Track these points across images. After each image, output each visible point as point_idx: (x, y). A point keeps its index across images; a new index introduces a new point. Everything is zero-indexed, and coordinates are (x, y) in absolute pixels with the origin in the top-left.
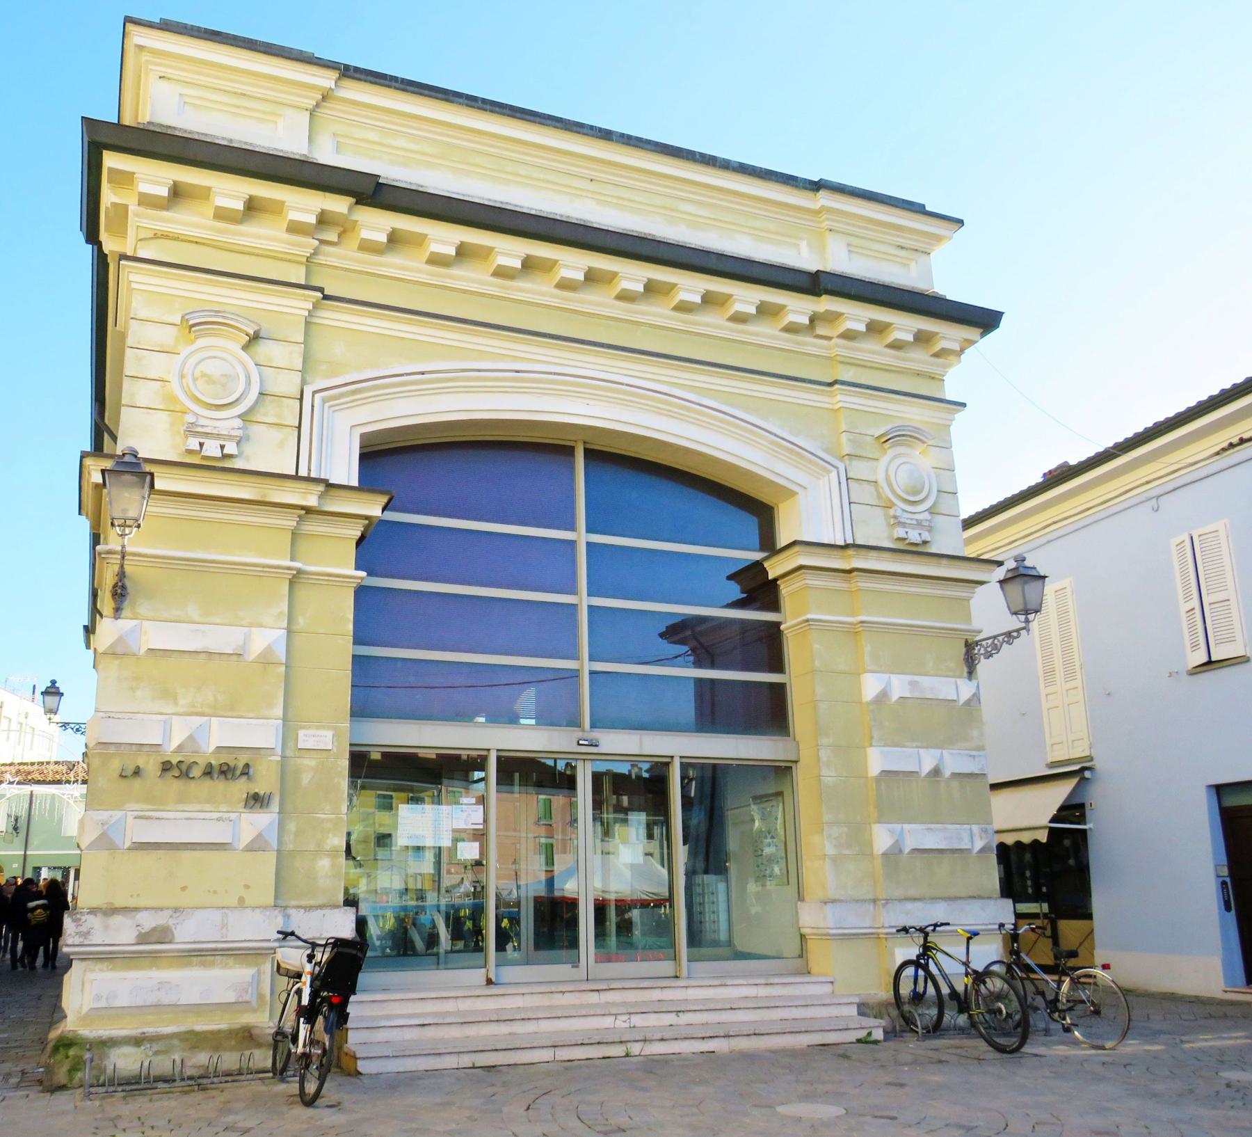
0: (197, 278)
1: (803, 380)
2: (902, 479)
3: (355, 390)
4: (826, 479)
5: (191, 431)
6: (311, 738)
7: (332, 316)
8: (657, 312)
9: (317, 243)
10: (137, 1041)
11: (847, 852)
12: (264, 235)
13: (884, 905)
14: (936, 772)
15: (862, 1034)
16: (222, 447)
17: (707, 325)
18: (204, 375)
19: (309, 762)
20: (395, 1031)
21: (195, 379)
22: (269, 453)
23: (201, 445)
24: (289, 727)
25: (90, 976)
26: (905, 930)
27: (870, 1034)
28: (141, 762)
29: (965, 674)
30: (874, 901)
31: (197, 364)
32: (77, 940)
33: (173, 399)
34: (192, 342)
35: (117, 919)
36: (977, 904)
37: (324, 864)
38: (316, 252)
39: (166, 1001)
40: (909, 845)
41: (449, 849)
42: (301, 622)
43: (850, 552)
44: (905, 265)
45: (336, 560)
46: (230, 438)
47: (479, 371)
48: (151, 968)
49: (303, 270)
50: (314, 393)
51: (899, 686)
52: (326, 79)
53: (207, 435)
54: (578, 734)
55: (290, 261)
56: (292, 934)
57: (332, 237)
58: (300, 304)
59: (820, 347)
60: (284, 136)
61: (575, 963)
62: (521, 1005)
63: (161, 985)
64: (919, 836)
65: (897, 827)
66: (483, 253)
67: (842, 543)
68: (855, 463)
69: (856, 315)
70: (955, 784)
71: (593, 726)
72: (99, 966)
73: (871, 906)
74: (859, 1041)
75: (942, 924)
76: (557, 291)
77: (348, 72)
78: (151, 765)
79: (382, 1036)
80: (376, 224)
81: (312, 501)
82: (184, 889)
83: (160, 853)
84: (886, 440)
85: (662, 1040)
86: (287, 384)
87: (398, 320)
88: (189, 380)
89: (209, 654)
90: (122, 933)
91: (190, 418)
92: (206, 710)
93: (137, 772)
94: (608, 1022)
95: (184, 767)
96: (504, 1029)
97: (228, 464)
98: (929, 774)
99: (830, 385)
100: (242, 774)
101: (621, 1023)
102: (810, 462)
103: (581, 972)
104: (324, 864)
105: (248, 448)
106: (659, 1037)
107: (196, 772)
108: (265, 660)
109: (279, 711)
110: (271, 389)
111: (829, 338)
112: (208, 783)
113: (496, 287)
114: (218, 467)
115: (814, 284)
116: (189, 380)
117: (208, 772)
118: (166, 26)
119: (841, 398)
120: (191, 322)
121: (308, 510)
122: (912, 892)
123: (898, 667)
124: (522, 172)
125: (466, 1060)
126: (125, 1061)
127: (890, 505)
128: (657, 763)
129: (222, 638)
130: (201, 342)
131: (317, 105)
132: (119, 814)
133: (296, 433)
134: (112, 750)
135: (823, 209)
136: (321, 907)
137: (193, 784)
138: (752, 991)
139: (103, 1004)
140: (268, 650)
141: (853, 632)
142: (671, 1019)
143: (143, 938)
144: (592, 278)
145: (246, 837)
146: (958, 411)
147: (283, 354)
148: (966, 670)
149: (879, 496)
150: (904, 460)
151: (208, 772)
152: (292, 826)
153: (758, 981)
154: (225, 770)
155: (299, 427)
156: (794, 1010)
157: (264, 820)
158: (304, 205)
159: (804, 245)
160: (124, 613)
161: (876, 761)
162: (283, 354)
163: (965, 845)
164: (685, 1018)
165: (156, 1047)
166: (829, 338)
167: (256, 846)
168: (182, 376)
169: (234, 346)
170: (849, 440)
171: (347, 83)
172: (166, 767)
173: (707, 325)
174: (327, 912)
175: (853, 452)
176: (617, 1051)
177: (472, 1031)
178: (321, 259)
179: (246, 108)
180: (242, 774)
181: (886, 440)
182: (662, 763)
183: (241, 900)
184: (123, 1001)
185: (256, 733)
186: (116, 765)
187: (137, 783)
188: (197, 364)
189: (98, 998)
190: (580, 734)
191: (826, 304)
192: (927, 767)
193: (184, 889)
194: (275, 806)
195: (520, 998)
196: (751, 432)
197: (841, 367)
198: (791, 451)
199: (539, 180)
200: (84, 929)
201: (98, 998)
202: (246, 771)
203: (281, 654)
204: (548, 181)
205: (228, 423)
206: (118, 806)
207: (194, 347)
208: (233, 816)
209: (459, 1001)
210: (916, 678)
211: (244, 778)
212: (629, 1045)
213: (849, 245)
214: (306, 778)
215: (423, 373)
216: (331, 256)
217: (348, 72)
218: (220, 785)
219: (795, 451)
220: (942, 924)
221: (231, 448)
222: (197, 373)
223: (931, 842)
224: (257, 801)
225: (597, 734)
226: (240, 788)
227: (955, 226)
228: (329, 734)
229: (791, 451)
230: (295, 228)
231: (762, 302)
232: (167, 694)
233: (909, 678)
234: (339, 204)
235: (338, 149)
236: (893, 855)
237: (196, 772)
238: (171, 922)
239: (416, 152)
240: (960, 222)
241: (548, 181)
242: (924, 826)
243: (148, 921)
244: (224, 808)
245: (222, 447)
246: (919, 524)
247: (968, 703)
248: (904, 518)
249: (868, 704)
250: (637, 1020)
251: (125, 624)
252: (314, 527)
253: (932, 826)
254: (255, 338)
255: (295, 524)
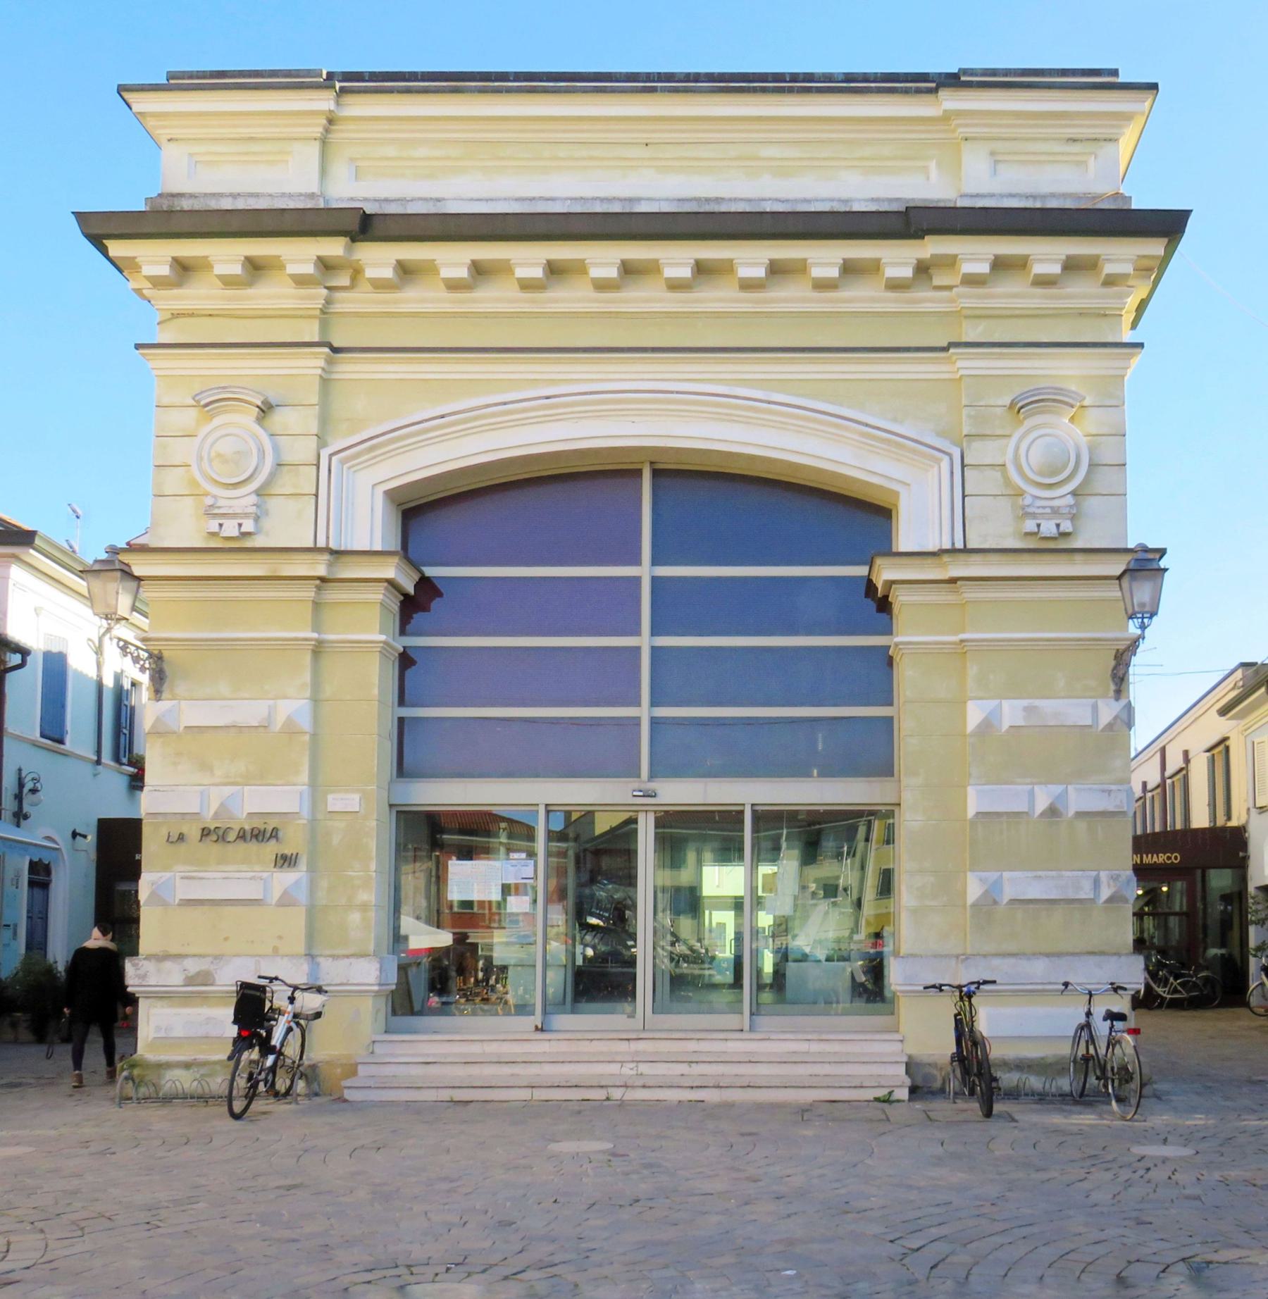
0: (208, 354)
1: (907, 349)
2: (1036, 456)
3: (372, 446)
4: (936, 469)
5: (210, 512)
6: (344, 801)
7: (349, 368)
8: (716, 297)
9: (325, 291)
10: (187, 1066)
11: (932, 903)
12: (271, 294)
13: (963, 961)
14: (1053, 812)
15: (881, 1093)
16: (1058, 526)
17: (786, 300)
18: (219, 455)
19: (340, 824)
20: (402, 1068)
21: (210, 461)
22: (289, 525)
23: (1039, 525)
24: (316, 788)
25: (153, 1011)
26: (939, 988)
27: (890, 1093)
28: (185, 830)
29: (1112, 693)
30: (957, 957)
31: (212, 445)
32: (136, 982)
33: (193, 483)
34: (1021, 422)
35: (168, 965)
36: (1092, 960)
37: (355, 917)
38: (328, 302)
39: (214, 1034)
40: (1008, 893)
41: (499, 904)
42: (328, 691)
43: (946, 558)
44: (1078, 163)
45: (367, 626)
46: (246, 515)
47: (505, 404)
48: (202, 1005)
49: (316, 325)
50: (331, 456)
51: (1011, 713)
52: (323, 101)
53: (224, 515)
54: (632, 784)
55: (301, 317)
56: (276, 979)
57: (344, 280)
58: (311, 364)
59: (940, 301)
60: (290, 178)
61: (632, 1015)
62: (547, 1050)
63: (209, 1019)
64: (1020, 884)
65: (993, 876)
66: (503, 268)
67: (936, 549)
68: (977, 445)
69: (975, 254)
70: (1082, 826)
71: (653, 775)
72: (159, 1003)
73: (953, 961)
74: (877, 1100)
75: (985, 982)
76: (816, 295)
77: (352, 82)
78: (193, 832)
79: (388, 1071)
80: (379, 259)
81: (321, 571)
82: (226, 939)
83: (205, 908)
84: (1018, 408)
85: (644, 1087)
86: (302, 450)
87: (558, 362)
88: (205, 464)
89: (240, 729)
90: (172, 976)
91: (209, 501)
92: (239, 780)
93: (181, 838)
94: (614, 1068)
95: (221, 833)
96: (507, 1070)
97: (1063, 545)
98: (1042, 814)
99: (945, 349)
100: (271, 836)
101: (627, 1070)
102: (914, 451)
103: (637, 1023)
104: (355, 917)
105: (266, 523)
106: (640, 1083)
107: (232, 836)
108: (290, 730)
109: (304, 777)
110: (287, 458)
111: (949, 288)
112: (242, 846)
113: (1038, 299)
114: (239, 548)
115: (910, 222)
116: (205, 464)
117: (242, 836)
118: (179, 82)
119: (967, 364)
120: (203, 403)
121: (323, 580)
122: (1012, 947)
123: (1013, 690)
124: (561, 155)
125: (445, 1095)
126: (183, 1080)
127: (1020, 494)
128: (666, 812)
129: (249, 711)
130: (1029, 423)
131: (327, 131)
132: (168, 875)
133: (313, 501)
134: (160, 819)
135: (947, 117)
136: (347, 957)
137: (230, 847)
138: (803, 1047)
139: (162, 1034)
140: (289, 721)
141: (962, 650)
142: (683, 1068)
143: (190, 981)
144: (406, 271)
145: (276, 894)
146: (1132, 355)
147: (297, 421)
148: (1112, 687)
149: (1007, 481)
150: (1042, 432)
151: (242, 836)
152: (324, 884)
153: (809, 1037)
154: (258, 835)
155: (964, 497)
156: (827, 1066)
157: (286, 879)
158: (300, 255)
159: (933, 165)
160: (164, 696)
161: (974, 801)
162: (297, 421)
163: (1086, 892)
164: (697, 1069)
165: (203, 1071)
166: (949, 288)
167: (286, 901)
168: (200, 458)
169: (247, 419)
170: (969, 416)
171: (349, 99)
172: (205, 833)
173: (786, 300)
174: (352, 960)
175: (973, 432)
176: (599, 1094)
177: (474, 1070)
178: (337, 308)
179: (254, 153)
180: (271, 836)
181: (1018, 408)
182: (589, 812)
183: (275, 950)
184: (178, 1032)
185: (279, 798)
186: (164, 832)
187: (182, 847)
188: (212, 445)
189: (158, 1029)
190: (636, 786)
191: (932, 247)
192: (1041, 805)
193: (226, 939)
194: (303, 864)
195: (547, 1044)
196: (836, 426)
197: (965, 323)
198: (888, 441)
199: (584, 159)
200: (141, 972)
201: (158, 1029)
202: (275, 834)
203: (305, 723)
204: (591, 158)
205: (244, 500)
206: (166, 868)
207: (1022, 430)
208: (265, 875)
209: (485, 1044)
210: (1037, 702)
211: (273, 841)
212: (610, 1090)
213: (992, 154)
214: (336, 840)
215: (442, 417)
216: (347, 302)
217: (352, 82)
218: (253, 846)
219: (894, 442)
220: (985, 982)
221: (1066, 526)
222: (213, 454)
223: (1035, 891)
224: (286, 861)
225: (655, 785)
226: (271, 849)
227: (1149, 96)
228: (356, 797)
229: (888, 441)
230: (301, 281)
231: (1068, 257)
232: (205, 767)
233: (1025, 702)
234: (334, 247)
235: (358, 175)
236: (988, 902)
237: (232, 836)
238: (212, 968)
239: (437, 159)
240: (1154, 87)
241: (591, 158)
242: (1030, 874)
243: (193, 966)
244: (257, 868)
245: (1058, 526)
246: (1055, 511)
247: (1110, 726)
248: (225, 505)
249: (971, 735)
250: (644, 1068)
251: (165, 705)
252: (333, 595)
253: (1040, 873)
254: (266, 410)
255: (313, 594)
